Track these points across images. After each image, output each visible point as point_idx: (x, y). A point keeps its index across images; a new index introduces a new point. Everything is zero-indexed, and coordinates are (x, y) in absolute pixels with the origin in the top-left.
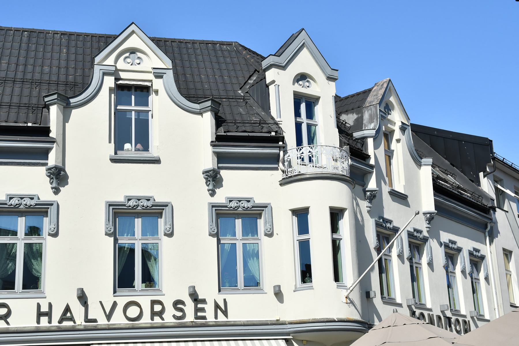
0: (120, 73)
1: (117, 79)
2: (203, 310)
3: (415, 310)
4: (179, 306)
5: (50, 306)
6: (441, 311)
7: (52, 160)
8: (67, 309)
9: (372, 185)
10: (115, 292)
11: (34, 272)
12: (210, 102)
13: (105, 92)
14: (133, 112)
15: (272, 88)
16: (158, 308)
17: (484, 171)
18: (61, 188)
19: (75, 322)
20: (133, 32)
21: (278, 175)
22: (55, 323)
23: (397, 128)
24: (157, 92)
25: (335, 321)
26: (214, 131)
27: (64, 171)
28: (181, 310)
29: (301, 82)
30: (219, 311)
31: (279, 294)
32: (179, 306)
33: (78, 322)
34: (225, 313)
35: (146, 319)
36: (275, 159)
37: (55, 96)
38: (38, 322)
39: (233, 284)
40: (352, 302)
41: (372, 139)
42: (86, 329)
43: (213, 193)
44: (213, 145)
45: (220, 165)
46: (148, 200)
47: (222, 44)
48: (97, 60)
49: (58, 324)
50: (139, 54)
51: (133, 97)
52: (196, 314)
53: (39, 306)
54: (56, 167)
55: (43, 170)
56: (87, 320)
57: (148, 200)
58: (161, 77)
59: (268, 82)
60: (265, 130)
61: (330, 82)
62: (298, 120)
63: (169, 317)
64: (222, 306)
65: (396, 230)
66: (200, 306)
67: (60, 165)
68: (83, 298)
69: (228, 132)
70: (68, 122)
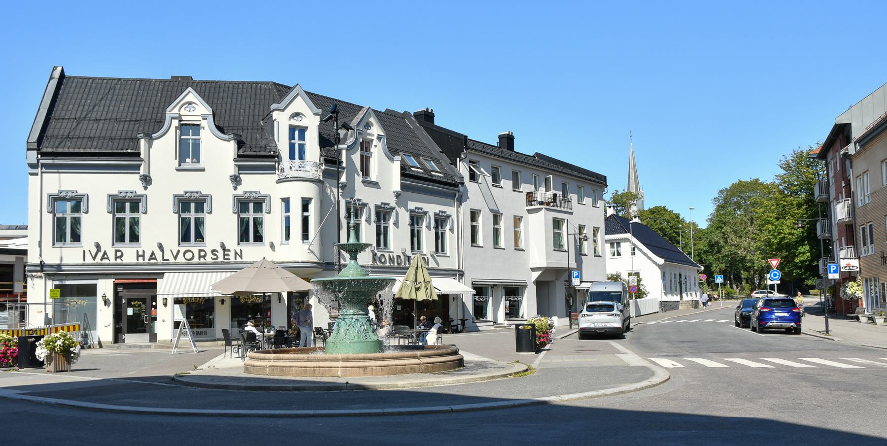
0: (182, 117)
1: (180, 121)
2: (228, 255)
3: (376, 252)
4: (214, 253)
5: (144, 251)
6: (402, 253)
7: (142, 171)
8: (153, 254)
9: (343, 179)
10: (179, 244)
11: (136, 232)
12: (233, 135)
13: (173, 129)
14: (191, 140)
15: (275, 122)
16: (202, 254)
17: (460, 157)
18: (148, 187)
19: (157, 261)
20: (190, 92)
21: (275, 177)
22: (146, 261)
23: (375, 138)
24: (204, 128)
25: (299, 262)
26: (237, 152)
27: (150, 177)
28: (215, 255)
29: (295, 118)
30: (240, 255)
31: (272, 246)
32: (214, 253)
33: (159, 261)
34: (241, 256)
35: (196, 260)
36: (273, 168)
37: (142, 134)
38: (138, 260)
39: (248, 240)
40: (312, 252)
41: (345, 150)
42: (163, 264)
43: (235, 188)
44: (235, 160)
45: (240, 172)
46: (197, 193)
47: (262, 83)
48: (168, 110)
49: (148, 261)
50: (194, 105)
51: (191, 131)
52: (224, 257)
53: (138, 252)
54: (144, 176)
55: (137, 176)
56: (163, 259)
57: (197, 193)
58: (206, 119)
59: (273, 119)
60: (267, 150)
61: (316, 116)
62: (293, 141)
63: (209, 258)
64: (239, 253)
65: (365, 205)
66: (226, 253)
67: (147, 174)
68: (161, 247)
69: (245, 152)
70: (151, 148)
